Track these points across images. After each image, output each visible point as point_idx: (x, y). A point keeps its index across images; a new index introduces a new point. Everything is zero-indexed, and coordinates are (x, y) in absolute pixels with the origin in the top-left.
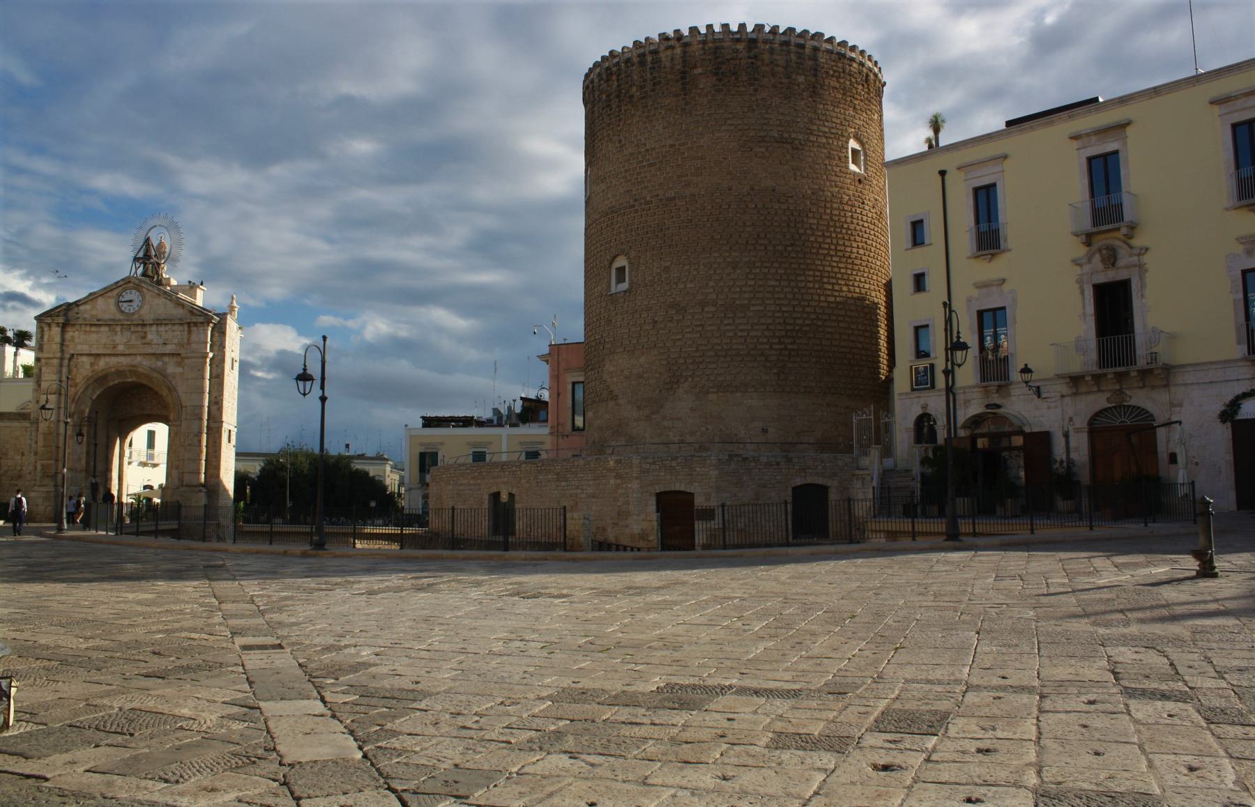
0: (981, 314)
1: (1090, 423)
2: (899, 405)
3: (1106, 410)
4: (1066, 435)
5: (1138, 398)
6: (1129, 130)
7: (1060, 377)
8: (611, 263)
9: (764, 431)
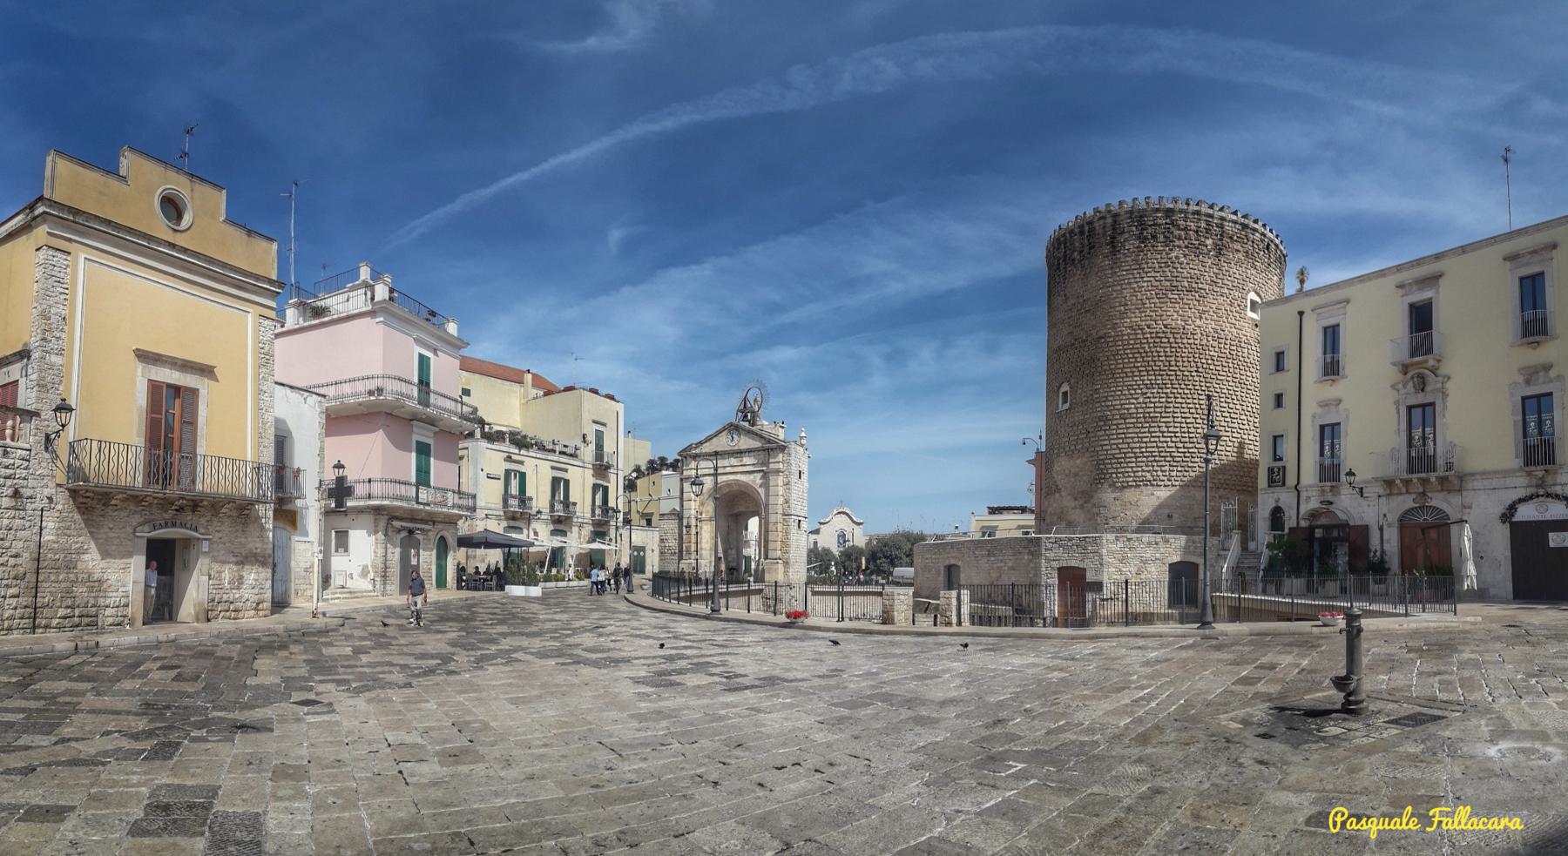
0: (1322, 427)
1: (1400, 520)
4: (1381, 529)
5: (1437, 500)
6: (1441, 281)
7: (1376, 479)
9: (1170, 516)
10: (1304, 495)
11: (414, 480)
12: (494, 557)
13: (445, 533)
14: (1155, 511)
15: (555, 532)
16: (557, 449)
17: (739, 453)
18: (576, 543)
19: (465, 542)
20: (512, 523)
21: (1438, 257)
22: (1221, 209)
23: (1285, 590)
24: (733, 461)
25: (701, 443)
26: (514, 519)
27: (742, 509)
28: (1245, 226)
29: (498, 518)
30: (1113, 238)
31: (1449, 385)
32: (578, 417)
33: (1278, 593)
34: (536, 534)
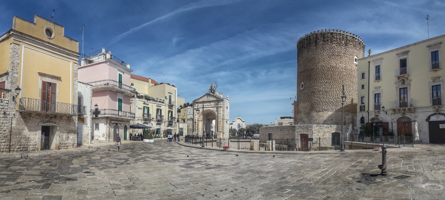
0: (375, 94)
1: (397, 121)
2: (358, 114)
4: (392, 123)
5: (408, 115)
6: (409, 53)
7: (391, 109)
9: (332, 120)
10: (370, 114)
11: (117, 109)
12: (140, 131)
15: (157, 124)
17: (210, 102)
18: (164, 127)
20: (145, 122)
21: (408, 46)
22: (347, 33)
23: (365, 140)
24: (208, 104)
25: (199, 99)
26: (146, 120)
27: (210, 117)
28: (353, 38)
29: (141, 120)
31: (411, 82)
32: (164, 92)
33: (363, 141)
34: (152, 124)
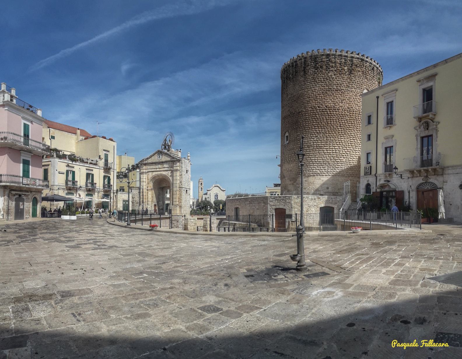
3: (422, 183)
4: (409, 192)
5: (432, 179)
6: (437, 77)
7: (407, 171)
8: (285, 135)
10: (378, 178)
11: (21, 175)
12: (61, 204)
13: (36, 196)
14: (321, 186)
15: (87, 195)
16: (89, 162)
17: (162, 163)
18: (97, 199)
19: (45, 199)
20: (69, 191)
21: (435, 66)
22: (352, 53)
23: (368, 217)
24: (160, 166)
25: (148, 159)
26: (70, 190)
27: (164, 185)
28: (362, 60)
29: (63, 189)
30: (305, 68)
31: (439, 126)
32: (97, 149)
33: (365, 219)
34: (80, 196)
